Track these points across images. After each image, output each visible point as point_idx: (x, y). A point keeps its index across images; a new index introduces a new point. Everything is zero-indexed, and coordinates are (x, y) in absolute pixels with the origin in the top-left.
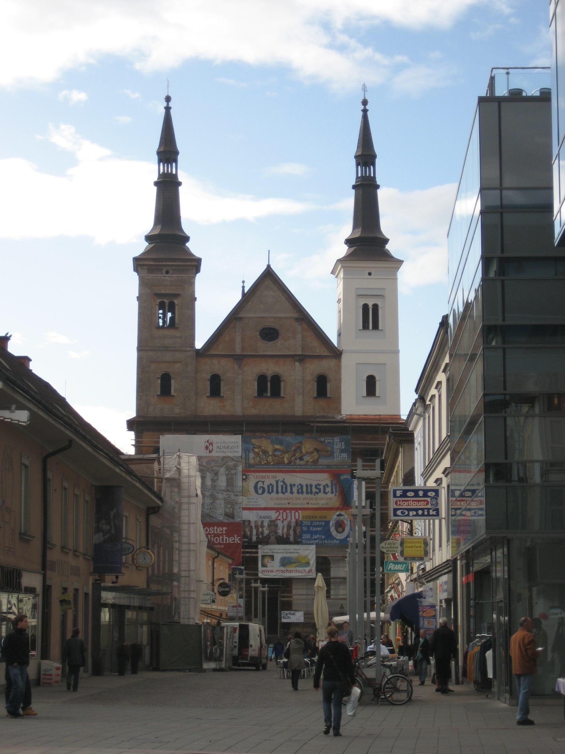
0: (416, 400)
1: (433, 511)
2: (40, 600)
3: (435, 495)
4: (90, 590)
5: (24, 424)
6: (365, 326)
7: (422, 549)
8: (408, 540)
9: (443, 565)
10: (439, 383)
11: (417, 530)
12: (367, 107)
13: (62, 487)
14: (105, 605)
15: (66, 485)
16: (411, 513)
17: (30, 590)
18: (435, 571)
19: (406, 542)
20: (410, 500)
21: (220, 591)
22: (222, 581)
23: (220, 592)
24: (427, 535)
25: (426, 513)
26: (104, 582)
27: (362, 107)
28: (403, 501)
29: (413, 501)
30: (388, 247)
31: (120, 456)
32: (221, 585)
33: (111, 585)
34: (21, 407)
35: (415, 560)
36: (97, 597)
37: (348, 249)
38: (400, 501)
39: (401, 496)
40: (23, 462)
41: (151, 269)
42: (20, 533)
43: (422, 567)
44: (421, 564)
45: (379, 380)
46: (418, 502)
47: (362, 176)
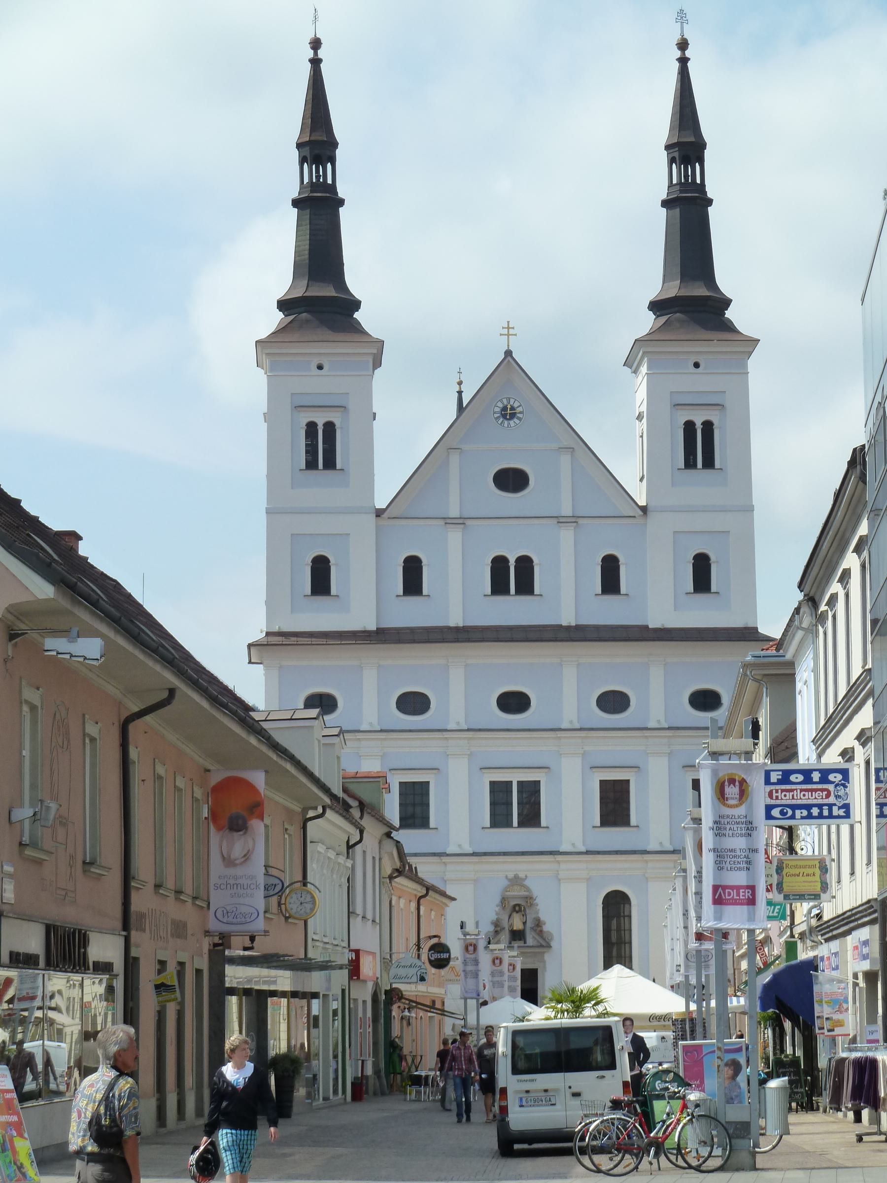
0: (800, 603)
1: (840, 808)
2: (119, 985)
3: (843, 779)
4: (203, 963)
5: (95, 663)
6: (690, 463)
7: (817, 878)
8: (791, 863)
9: (861, 909)
10: (846, 573)
11: (803, 843)
12: (688, 53)
13: (154, 775)
14: (232, 991)
15: (161, 770)
16: (798, 812)
17: (103, 968)
18: (843, 919)
19: (787, 866)
20: (797, 789)
21: (433, 959)
22: (434, 941)
23: (433, 961)
24: (825, 852)
25: (826, 813)
26: (229, 948)
27: (678, 54)
28: (783, 791)
29: (801, 790)
30: (729, 314)
31: (251, 713)
32: (433, 948)
33: (242, 953)
34: (93, 633)
35: (805, 899)
36: (218, 976)
37: (655, 319)
38: (777, 791)
39: (779, 782)
40: (86, 731)
42: (84, 863)
43: (815, 911)
44: (815, 907)
46: (810, 793)
47: (680, 183)
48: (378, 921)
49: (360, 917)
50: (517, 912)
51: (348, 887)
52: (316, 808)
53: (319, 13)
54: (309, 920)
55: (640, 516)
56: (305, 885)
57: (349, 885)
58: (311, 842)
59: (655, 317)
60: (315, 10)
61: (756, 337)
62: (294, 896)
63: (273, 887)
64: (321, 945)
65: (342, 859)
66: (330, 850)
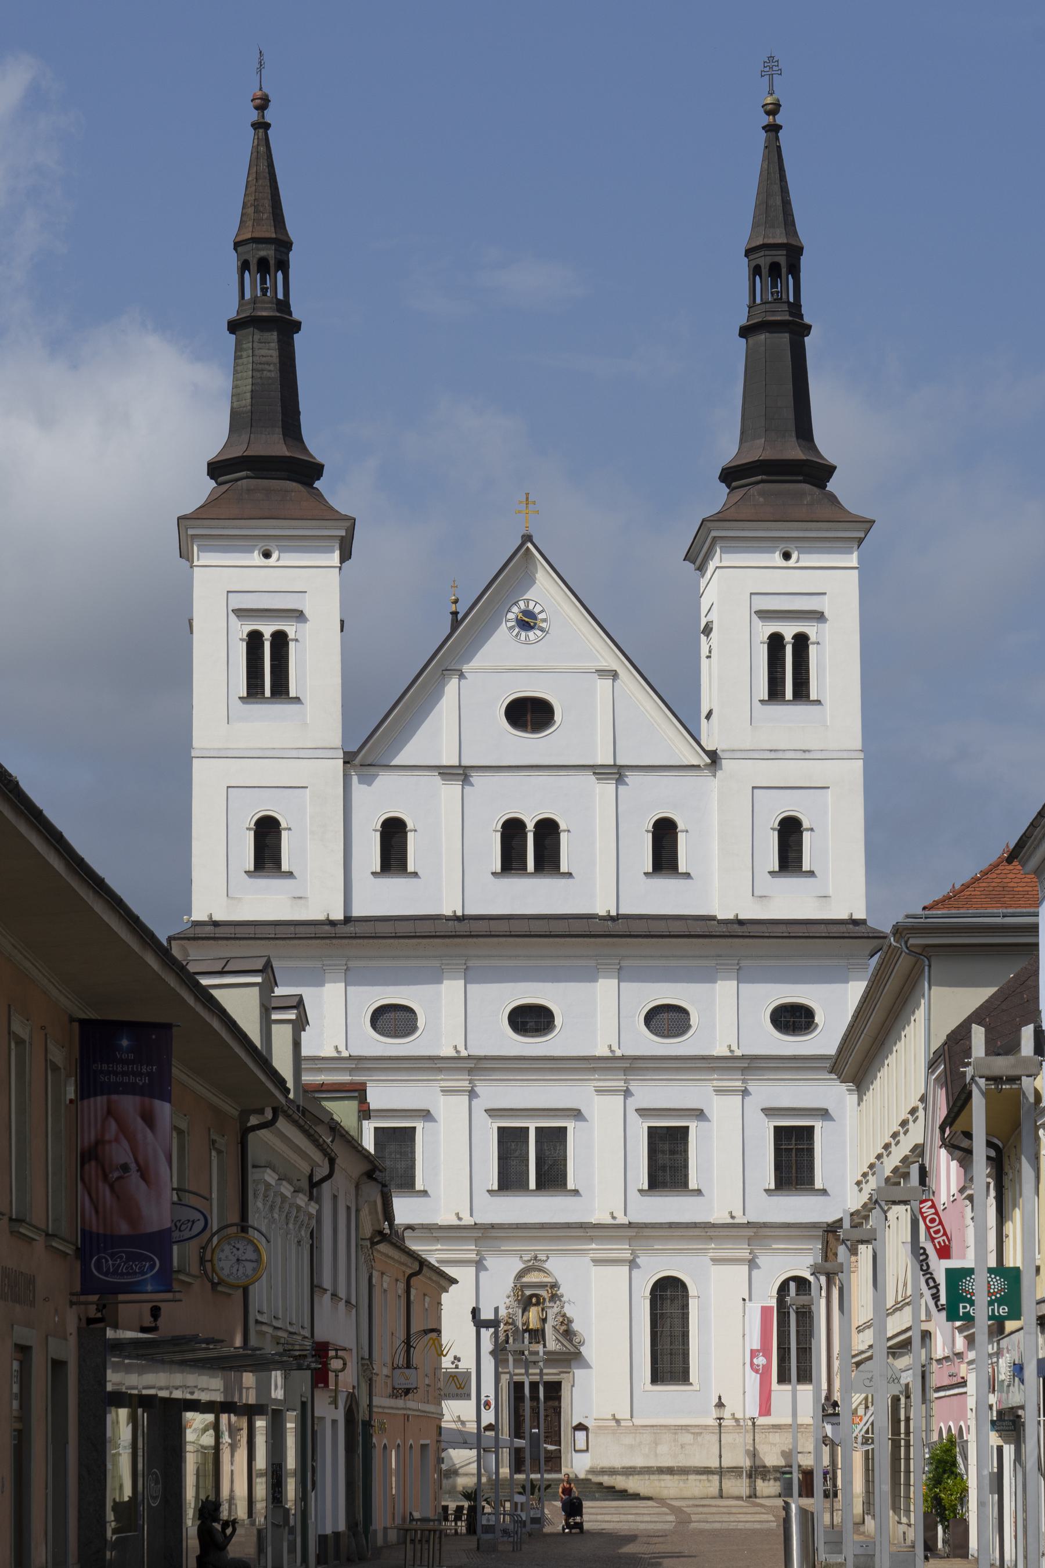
4: (69, 1351)
6: (775, 692)
14: (119, 1399)
41: (445, 1288)
45: (812, 830)
48: (354, 1302)
49: (329, 1293)
50: (535, 1305)
51: (312, 1246)
52: (261, 1111)
53: (266, 58)
54: (251, 1288)
55: (706, 765)
56: (244, 1229)
57: (313, 1242)
58: (254, 1166)
59: (728, 490)
60: (261, 52)
61: (869, 516)
62: (227, 1248)
63: (190, 1224)
64: (270, 1330)
65: (301, 1200)
66: (284, 1183)
